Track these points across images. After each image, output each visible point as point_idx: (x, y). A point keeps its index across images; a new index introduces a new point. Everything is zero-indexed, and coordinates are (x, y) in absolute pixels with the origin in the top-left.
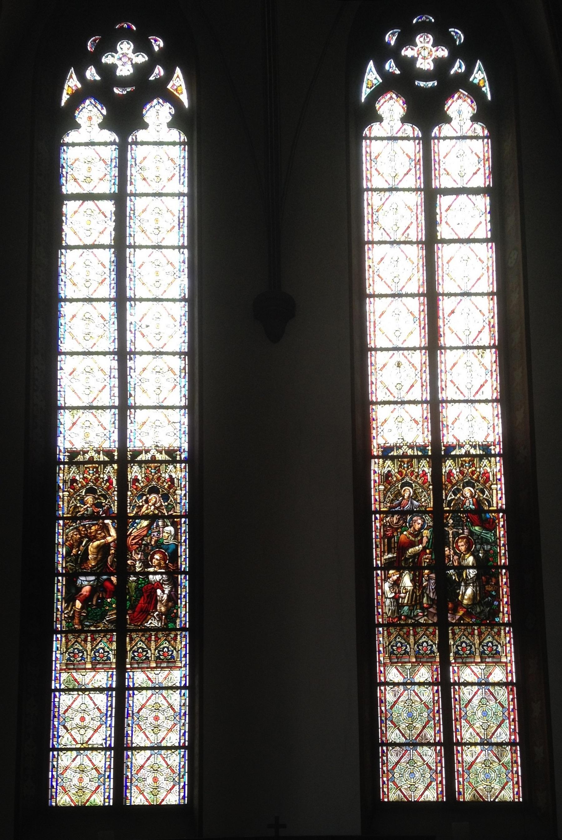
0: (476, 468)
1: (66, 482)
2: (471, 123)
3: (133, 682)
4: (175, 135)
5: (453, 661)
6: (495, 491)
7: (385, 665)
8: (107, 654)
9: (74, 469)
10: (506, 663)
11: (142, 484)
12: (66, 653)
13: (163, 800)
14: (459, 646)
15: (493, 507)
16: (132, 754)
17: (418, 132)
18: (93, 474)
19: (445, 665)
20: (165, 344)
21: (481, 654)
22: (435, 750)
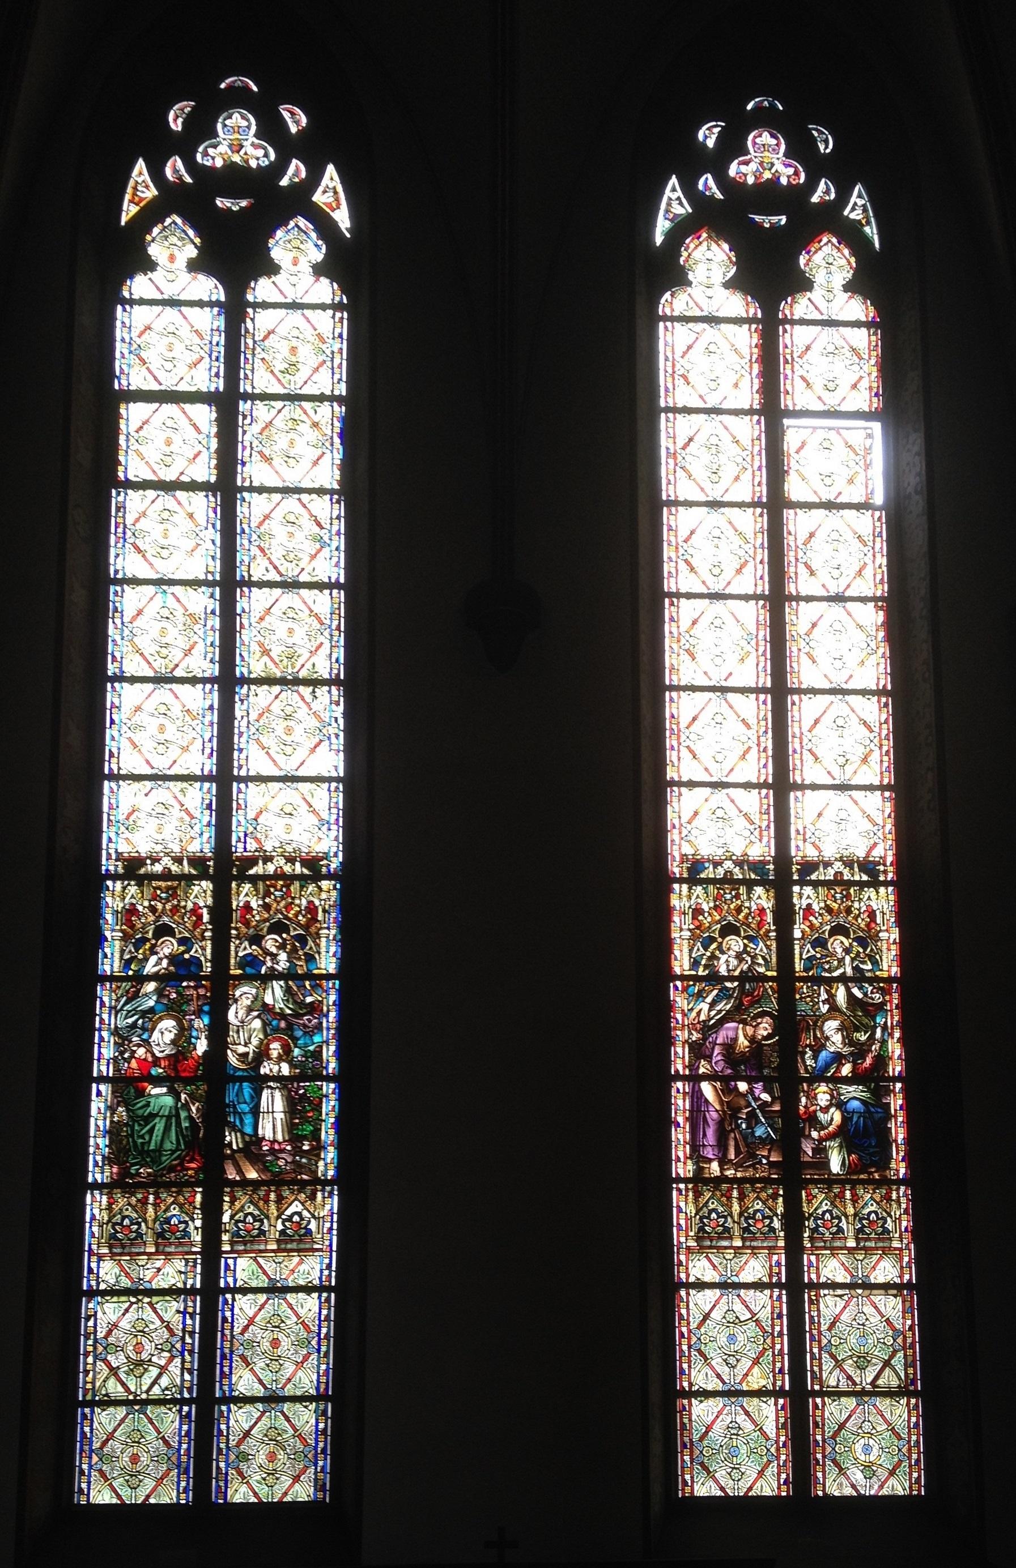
0: (179, 901)
1: (684, 913)
2: (313, 279)
3: (234, 1276)
4: (325, 290)
5: (809, 1245)
6: (324, 940)
7: (100, 1258)
8: (136, 1227)
9: (133, 889)
10: (901, 1249)
11: (257, 918)
12: (107, 1224)
13: (285, 1494)
14: (241, 1221)
15: (882, 970)
16: (229, 1410)
17: (754, 310)
18: (842, 899)
19: (794, 1251)
20: (825, 676)
21: (813, 1234)
22: (180, 1411)
